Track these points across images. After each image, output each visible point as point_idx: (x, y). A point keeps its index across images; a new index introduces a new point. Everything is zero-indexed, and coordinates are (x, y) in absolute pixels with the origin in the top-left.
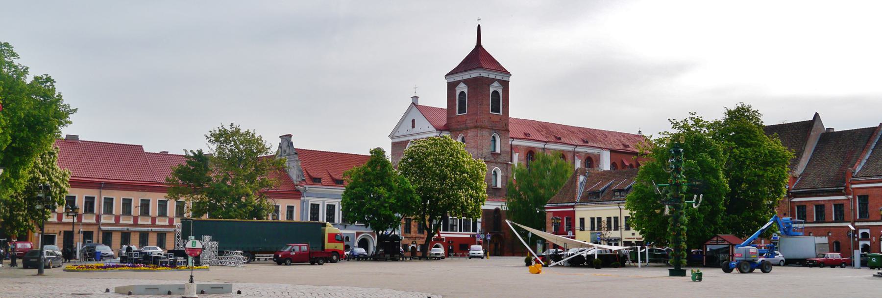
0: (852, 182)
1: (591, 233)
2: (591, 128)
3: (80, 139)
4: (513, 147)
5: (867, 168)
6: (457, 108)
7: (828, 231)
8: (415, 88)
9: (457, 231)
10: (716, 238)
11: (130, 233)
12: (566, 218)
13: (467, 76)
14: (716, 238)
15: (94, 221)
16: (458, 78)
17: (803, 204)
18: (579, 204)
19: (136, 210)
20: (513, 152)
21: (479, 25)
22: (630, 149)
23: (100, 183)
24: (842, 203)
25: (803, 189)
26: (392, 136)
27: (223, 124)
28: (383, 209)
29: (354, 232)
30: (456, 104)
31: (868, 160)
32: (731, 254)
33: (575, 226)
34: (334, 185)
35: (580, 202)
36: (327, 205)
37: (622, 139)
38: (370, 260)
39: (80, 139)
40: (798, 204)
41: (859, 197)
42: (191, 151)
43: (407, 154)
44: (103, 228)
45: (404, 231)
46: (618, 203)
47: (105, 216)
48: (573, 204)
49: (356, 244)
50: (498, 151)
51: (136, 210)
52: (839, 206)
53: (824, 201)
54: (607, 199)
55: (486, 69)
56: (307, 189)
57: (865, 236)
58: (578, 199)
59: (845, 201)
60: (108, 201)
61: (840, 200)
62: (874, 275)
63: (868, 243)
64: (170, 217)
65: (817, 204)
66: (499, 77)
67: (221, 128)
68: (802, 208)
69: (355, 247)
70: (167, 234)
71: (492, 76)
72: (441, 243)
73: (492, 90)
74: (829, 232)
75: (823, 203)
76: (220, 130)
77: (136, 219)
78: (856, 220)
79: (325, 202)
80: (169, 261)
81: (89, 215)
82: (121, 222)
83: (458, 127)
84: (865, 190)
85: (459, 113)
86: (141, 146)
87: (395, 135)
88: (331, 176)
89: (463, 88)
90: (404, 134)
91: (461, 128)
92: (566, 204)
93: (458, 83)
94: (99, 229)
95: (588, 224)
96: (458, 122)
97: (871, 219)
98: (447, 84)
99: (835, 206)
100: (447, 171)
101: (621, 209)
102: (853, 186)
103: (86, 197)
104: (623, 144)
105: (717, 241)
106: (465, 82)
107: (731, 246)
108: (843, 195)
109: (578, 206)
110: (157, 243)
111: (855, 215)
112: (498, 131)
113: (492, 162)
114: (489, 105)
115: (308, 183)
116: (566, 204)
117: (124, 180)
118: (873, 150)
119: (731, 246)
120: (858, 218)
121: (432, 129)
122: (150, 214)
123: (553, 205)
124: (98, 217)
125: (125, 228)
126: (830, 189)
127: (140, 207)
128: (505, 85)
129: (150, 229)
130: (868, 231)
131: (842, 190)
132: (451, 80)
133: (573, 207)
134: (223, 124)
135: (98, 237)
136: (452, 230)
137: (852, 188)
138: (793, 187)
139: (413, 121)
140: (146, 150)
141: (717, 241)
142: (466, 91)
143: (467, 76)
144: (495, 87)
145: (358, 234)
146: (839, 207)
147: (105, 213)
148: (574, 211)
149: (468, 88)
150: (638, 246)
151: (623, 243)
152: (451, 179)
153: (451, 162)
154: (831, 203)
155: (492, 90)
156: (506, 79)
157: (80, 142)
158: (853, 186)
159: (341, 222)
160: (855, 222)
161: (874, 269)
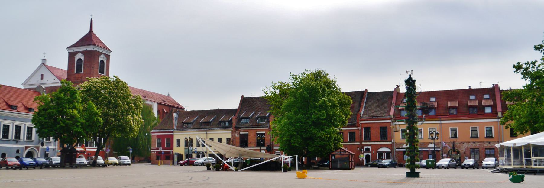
0: (360, 120)
1: (185, 149)
2: (145, 90)
9: (93, 146)
10: (339, 150)
12: (167, 139)
13: (84, 49)
14: (339, 150)
16: (77, 49)
18: (177, 130)
21: (92, 19)
22: (166, 103)
28: (75, 127)
29: (23, 146)
30: (74, 66)
31: (365, 108)
32: (350, 161)
33: (192, 143)
34: (11, 110)
35: (177, 129)
36: (4, 125)
37: (161, 97)
38: (57, 168)
41: (364, 128)
43: (86, 87)
46: (206, 130)
48: (173, 130)
49: (24, 156)
57: (367, 150)
58: (175, 127)
59: (356, 130)
62: (491, 172)
63: (370, 154)
66: (104, 52)
69: (23, 157)
71: (100, 51)
73: (100, 59)
78: (363, 141)
79: (14, 123)
83: (76, 81)
84: (368, 124)
85: (76, 72)
95: (182, 143)
99: (350, 133)
100: (119, 101)
101: (207, 134)
102: (361, 122)
104: (163, 100)
105: (340, 152)
106: (82, 52)
107: (350, 155)
108: (355, 127)
111: (362, 139)
114: (98, 69)
118: (366, 103)
119: (350, 155)
123: (157, 131)
128: (108, 57)
130: (370, 147)
131: (356, 124)
132: (72, 51)
133: (172, 132)
136: (90, 146)
137: (361, 123)
139: (42, 75)
141: (340, 152)
142: (83, 58)
143: (84, 49)
145: (26, 148)
148: (173, 135)
150: (296, 156)
151: (208, 155)
153: (122, 95)
155: (100, 59)
156: (108, 54)
158: (361, 122)
160: (362, 142)
161: (182, 165)
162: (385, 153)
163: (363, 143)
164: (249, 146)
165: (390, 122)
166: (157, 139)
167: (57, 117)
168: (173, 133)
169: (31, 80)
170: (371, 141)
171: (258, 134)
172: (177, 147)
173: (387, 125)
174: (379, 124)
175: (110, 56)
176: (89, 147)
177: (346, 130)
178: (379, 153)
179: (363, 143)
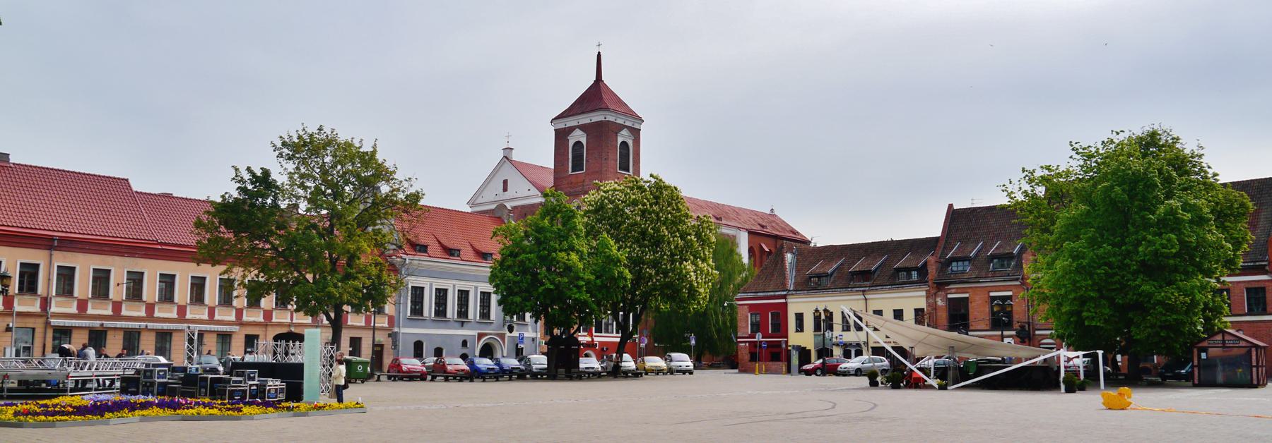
1: (815, 335)
3: (13, 160)
11: (106, 332)
13: (585, 119)
15: (36, 308)
16: (571, 122)
19: (117, 290)
21: (599, 53)
23: (51, 239)
24: (1263, 286)
27: (305, 126)
28: (575, 290)
29: (475, 333)
30: (568, 159)
32: (1254, 364)
37: (755, 217)
38: (542, 379)
39: (13, 160)
42: (249, 169)
43: (593, 203)
44: (55, 322)
45: (543, 331)
46: (864, 291)
47: (59, 299)
48: (785, 293)
49: (477, 353)
51: (117, 290)
54: (840, 285)
55: (614, 111)
56: (407, 262)
58: (791, 286)
60: (66, 272)
61: (1258, 281)
64: (180, 304)
65: (1250, 286)
66: (628, 124)
67: (301, 133)
70: (174, 334)
71: (620, 121)
72: (592, 350)
73: (620, 140)
76: (300, 137)
77: (117, 306)
79: (434, 284)
80: (248, 388)
81: (27, 297)
82: (90, 311)
85: (572, 171)
86: (127, 180)
87: (478, 201)
88: (440, 243)
89: (579, 136)
90: (490, 200)
91: (575, 192)
92: (772, 293)
93: (572, 129)
94: (47, 324)
95: (809, 322)
96: (571, 183)
98: (554, 132)
99: (1248, 290)
101: (866, 299)
103: (21, 264)
104: (759, 224)
105: (1223, 340)
106: (583, 128)
109: (791, 297)
110: (156, 350)
115: (408, 252)
116: (772, 293)
117: (97, 235)
119: (1253, 349)
121: (535, 191)
122: (145, 298)
124: (45, 302)
125: (96, 323)
127: (125, 285)
128: (636, 133)
129: (143, 324)
131: (1265, 265)
132: (561, 126)
133: (784, 297)
134: (305, 126)
135: (45, 338)
136: (607, 331)
139: (505, 182)
140: (136, 186)
141: (1223, 340)
142: (584, 141)
143: (585, 119)
144: (623, 136)
145: (480, 336)
147: (58, 294)
148: (785, 304)
150: (1098, 351)
151: (870, 350)
152: (669, 243)
154: (1242, 285)
155: (620, 140)
157: (12, 165)
159: (456, 317)
161: (810, 375)
166: (749, 314)
168: (786, 299)
172: (797, 331)
176: (603, 334)
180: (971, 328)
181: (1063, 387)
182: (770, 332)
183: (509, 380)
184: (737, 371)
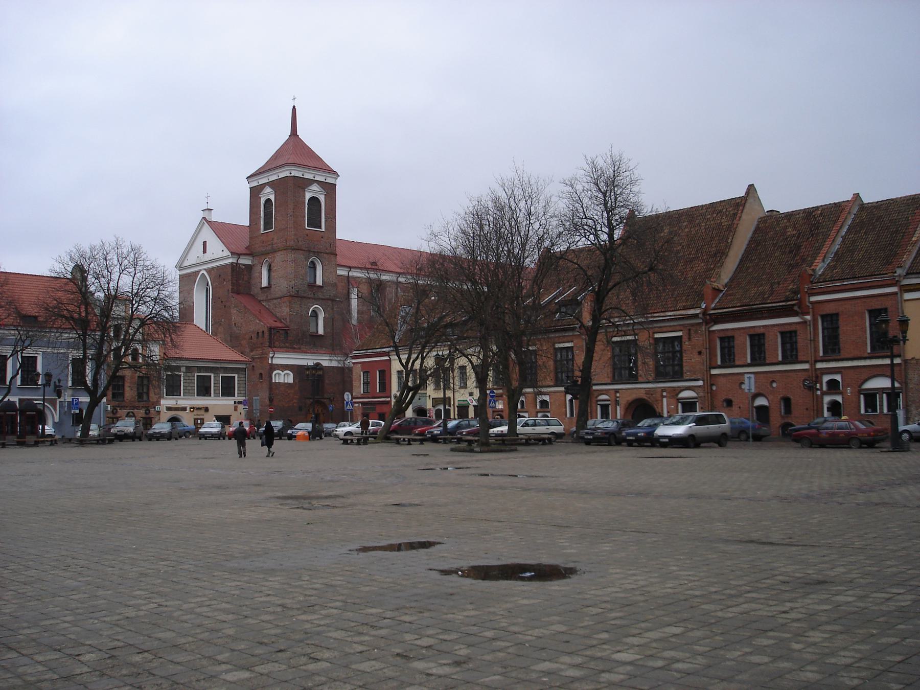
0: (809, 292)
4: (350, 279)
5: (835, 267)
6: (262, 223)
7: (771, 380)
8: (207, 197)
17: (729, 334)
20: (351, 287)
21: (294, 107)
25: (729, 308)
26: (180, 267)
40: (722, 335)
41: (823, 317)
50: (319, 282)
52: (788, 335)
53: (733, 329)
57: (833, 385)
63: (839, 399)
65: (752, 332)
66: (318, 178)
68: (727, 340)
71: (310, 176)
73: (308, 196)
74: (773, 381)
75: (762, 331)
78: (819, 359)
84: (832, 304)
89: (269, 194)
93: (262, 186)
97: (844, 354)
102: (813, 299)
106: (271, 184)
108: (795, 314)
111: (816, 350)
112: (318, 254)
113: (309, 298)
120: (821, 354)
126: (774, 305)
128: (330, 189)
130: (838, 378)
132: (255, 184)
137: (812, 303)
138: (713, 305)
142: (272, 198)
146: (789, 336)
149: (276, 192)
158: (813, 299)
160: (816, 361)
162: (885, 396)
163: (819, 365)
164: (737, 363)
165: (895, 294)
166: (362, 373)
167: (420, 319)
168: (389, 356)
169: (189, 257)
170: (842, 356)
171: (657, 340)
173: (888, 303)
174: (864, 300)
175: (860, 195)
177: (773, 326)
178: (866, 396)
179: (819, 365)
180: (594, 382)
181: (751, 439)
182: (378, 391)
183: (50, 445)
184: (799, 445)
